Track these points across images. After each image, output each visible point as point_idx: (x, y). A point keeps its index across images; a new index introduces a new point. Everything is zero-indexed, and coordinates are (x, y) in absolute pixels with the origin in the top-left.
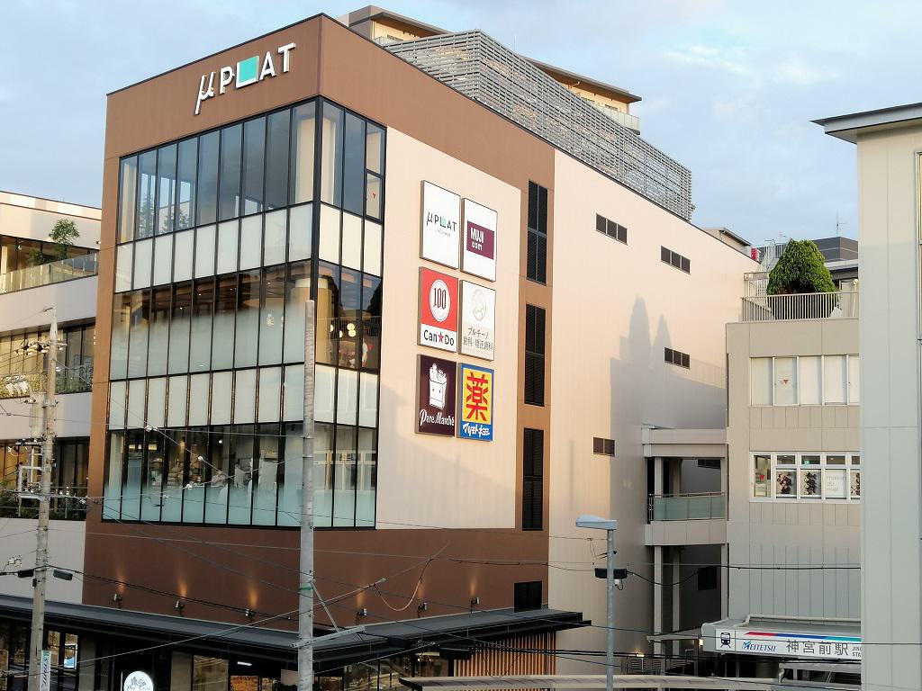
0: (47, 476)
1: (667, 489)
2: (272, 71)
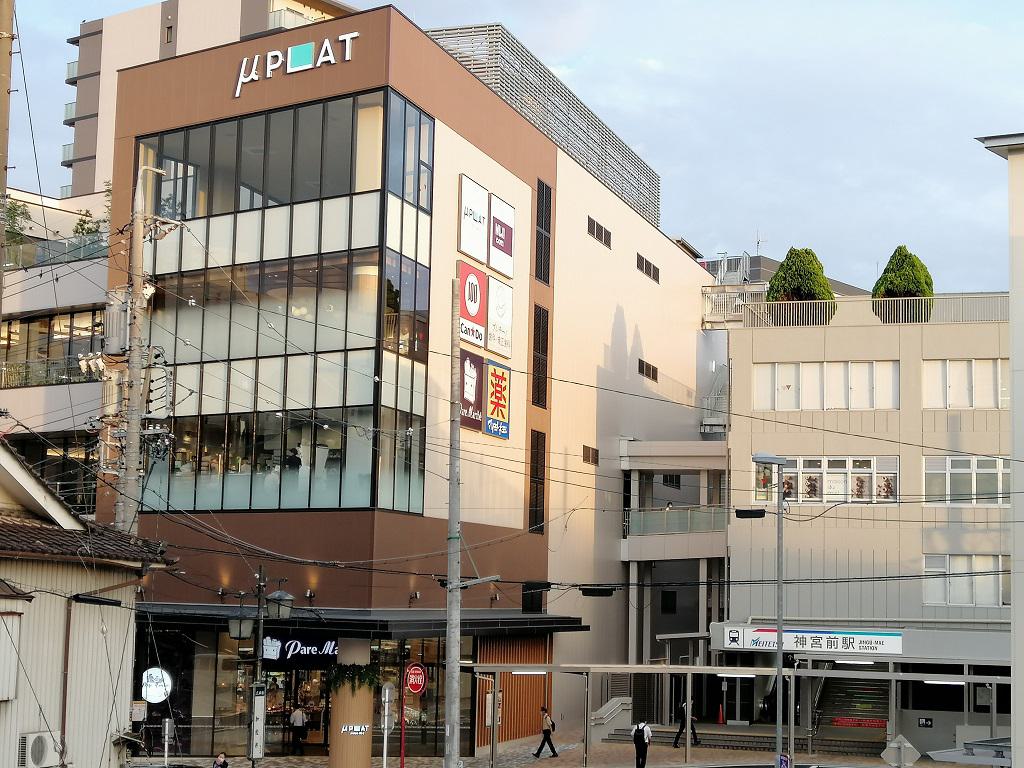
1: (642, 503)
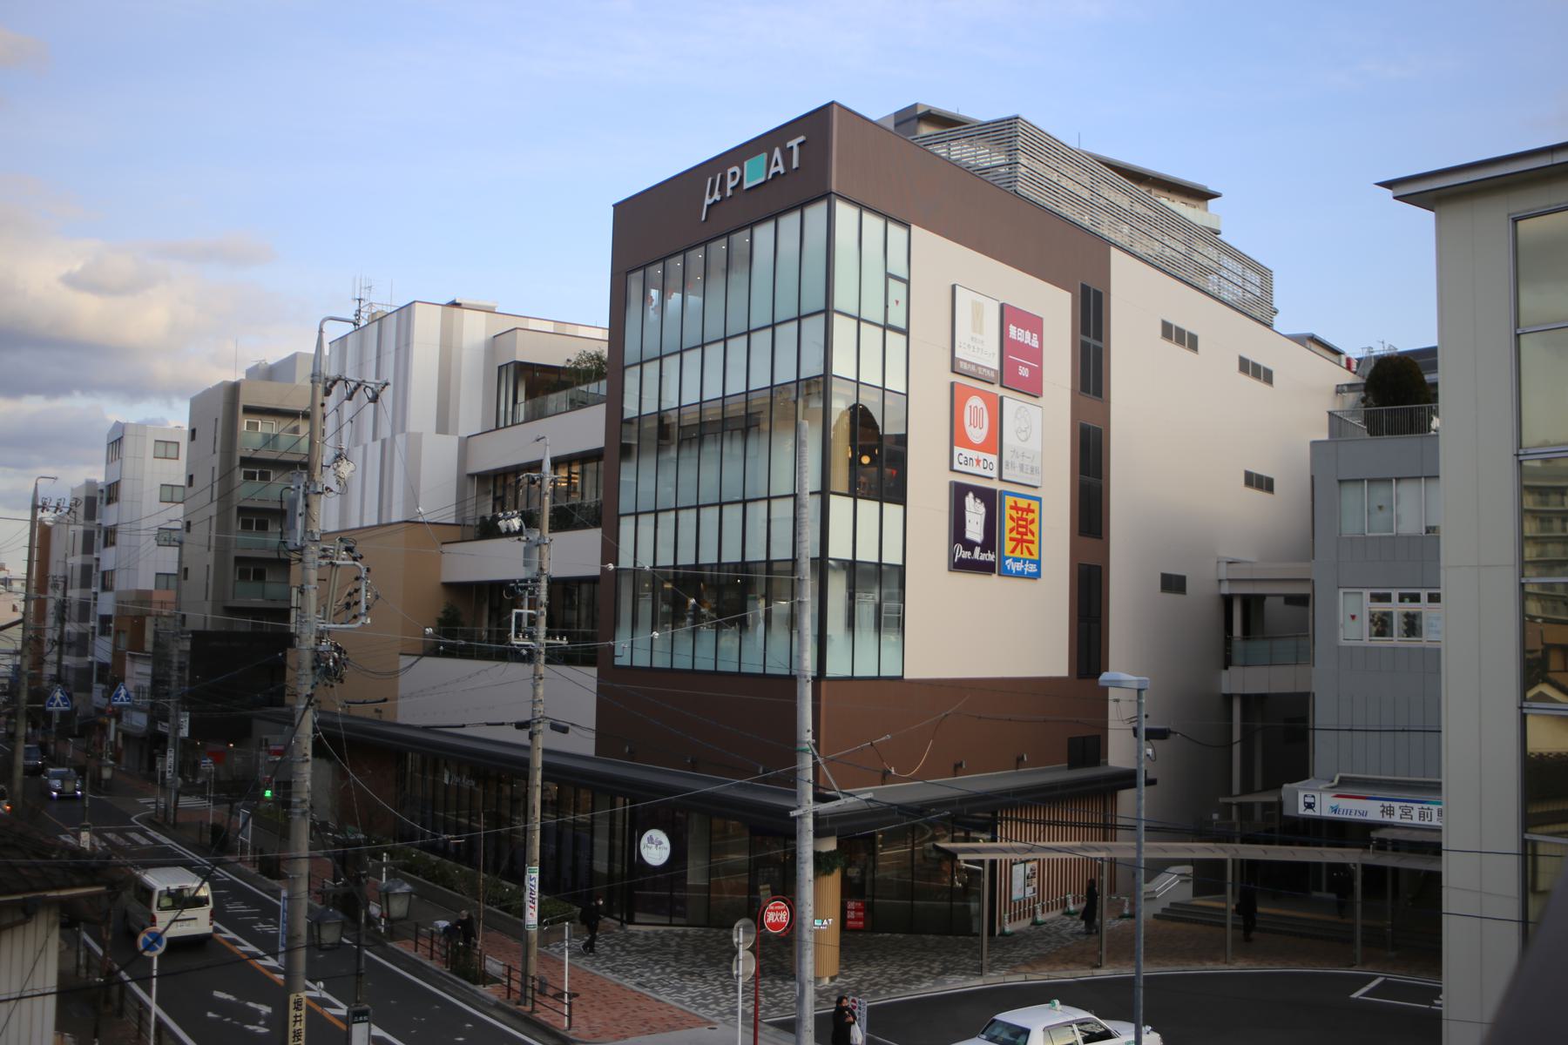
0: (543, 620)
2: (781, 169)
